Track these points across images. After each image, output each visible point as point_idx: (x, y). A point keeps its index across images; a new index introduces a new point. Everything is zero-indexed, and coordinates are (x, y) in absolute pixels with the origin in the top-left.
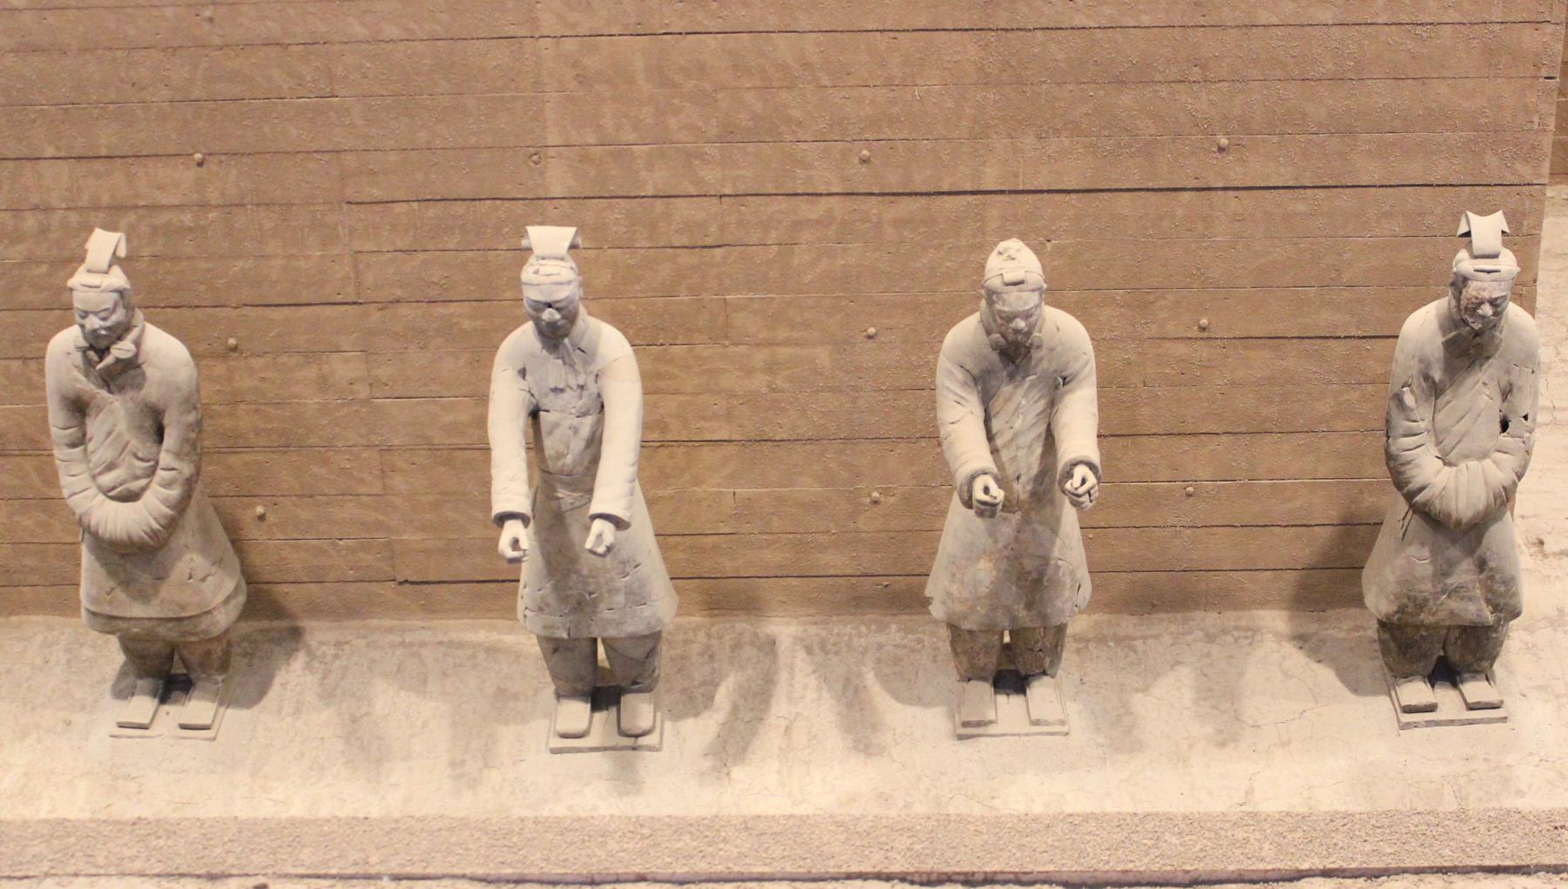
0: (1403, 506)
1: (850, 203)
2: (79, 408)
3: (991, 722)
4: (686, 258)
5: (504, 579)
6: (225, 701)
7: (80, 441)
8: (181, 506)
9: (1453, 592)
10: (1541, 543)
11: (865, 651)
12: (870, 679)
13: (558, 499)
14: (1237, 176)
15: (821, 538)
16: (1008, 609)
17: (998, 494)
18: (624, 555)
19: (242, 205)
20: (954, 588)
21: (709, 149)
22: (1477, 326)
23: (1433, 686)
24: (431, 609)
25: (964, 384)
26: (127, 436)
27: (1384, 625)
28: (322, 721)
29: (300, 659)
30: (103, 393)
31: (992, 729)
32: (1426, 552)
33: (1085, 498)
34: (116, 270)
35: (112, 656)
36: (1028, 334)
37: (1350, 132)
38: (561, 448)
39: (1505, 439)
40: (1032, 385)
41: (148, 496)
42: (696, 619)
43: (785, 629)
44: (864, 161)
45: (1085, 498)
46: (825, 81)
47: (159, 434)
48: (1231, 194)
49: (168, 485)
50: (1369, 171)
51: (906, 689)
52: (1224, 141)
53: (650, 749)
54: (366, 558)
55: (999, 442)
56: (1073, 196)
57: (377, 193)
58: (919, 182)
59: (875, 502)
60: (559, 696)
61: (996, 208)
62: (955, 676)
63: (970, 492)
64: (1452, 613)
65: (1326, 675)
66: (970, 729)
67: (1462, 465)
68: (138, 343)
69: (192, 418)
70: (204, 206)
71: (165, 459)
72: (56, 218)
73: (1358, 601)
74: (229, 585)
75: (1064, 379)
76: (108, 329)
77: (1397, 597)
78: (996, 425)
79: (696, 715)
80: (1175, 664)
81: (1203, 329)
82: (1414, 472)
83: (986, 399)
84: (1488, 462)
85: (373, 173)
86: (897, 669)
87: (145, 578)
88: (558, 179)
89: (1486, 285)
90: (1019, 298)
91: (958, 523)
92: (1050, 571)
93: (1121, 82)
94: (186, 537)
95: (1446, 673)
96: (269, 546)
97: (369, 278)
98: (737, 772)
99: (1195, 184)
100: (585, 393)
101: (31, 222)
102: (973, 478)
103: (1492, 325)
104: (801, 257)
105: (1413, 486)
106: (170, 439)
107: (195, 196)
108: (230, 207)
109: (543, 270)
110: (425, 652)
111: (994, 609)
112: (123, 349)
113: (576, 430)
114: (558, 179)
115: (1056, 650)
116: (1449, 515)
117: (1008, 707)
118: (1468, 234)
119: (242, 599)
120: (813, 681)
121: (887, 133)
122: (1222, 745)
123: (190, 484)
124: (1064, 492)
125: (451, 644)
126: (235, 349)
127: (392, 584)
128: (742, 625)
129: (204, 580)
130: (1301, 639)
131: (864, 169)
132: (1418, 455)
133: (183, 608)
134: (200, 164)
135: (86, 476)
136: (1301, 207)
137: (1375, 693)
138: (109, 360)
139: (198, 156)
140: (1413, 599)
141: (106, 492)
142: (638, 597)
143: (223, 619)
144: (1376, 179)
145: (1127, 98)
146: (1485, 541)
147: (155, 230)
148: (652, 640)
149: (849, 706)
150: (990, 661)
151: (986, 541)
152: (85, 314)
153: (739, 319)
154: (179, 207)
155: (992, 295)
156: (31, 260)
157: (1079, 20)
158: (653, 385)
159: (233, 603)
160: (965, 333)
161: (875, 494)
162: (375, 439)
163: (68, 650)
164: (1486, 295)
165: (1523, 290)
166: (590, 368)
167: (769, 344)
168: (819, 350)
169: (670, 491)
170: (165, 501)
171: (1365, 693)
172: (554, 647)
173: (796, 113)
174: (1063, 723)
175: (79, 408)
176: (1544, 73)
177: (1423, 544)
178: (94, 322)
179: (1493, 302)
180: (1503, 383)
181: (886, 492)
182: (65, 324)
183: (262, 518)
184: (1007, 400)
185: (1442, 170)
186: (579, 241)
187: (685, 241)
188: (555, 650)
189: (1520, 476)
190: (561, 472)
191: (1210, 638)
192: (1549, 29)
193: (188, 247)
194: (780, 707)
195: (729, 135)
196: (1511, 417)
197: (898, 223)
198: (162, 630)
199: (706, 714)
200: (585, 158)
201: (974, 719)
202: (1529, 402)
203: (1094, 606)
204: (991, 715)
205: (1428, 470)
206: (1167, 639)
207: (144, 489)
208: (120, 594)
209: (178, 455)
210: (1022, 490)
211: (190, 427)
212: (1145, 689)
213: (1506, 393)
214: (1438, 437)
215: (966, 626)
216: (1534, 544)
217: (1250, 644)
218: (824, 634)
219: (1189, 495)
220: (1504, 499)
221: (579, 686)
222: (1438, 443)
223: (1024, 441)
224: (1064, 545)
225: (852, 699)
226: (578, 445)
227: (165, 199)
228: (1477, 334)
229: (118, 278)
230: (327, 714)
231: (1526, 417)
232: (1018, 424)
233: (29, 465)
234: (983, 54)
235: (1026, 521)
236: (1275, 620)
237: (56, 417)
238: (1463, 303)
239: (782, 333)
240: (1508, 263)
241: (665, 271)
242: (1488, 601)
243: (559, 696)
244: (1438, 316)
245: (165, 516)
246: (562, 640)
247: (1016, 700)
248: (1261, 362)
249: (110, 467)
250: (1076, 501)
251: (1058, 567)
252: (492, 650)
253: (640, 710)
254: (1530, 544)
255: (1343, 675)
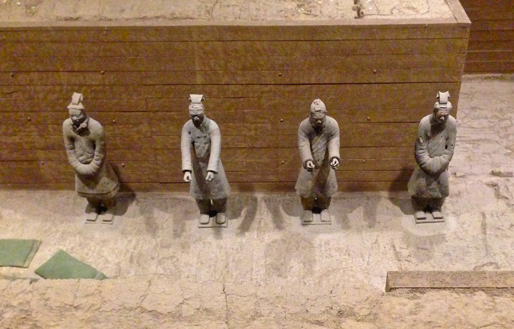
0: (419, 168)
1: (277, 87)
2: (72, 140)
3: (311, 221)
4: (232, 100)
5: (185, 186)
6: (115, 214)
7: (73, 148)
8: (101, 165)
9: (431, 190)
10: (455, 174)
11: (280, 201)
12: (281, 208)
13: (199, 165)
14: (379, 80)
15: (269, 173)
16: (316, 193)
17: (313, 166)
18: (217, 179)
19: (115, 85)
20: (302, 188)
21: (238, 72)
22: (440, 122)
23: (425, 212)
24: (169, 189)
25: (305, 137)
26: (86, 147)
27: (413, 197)
28: (140, 219)
29: (134, 203)
30: (79, 136)
31: (312, 223)
32: (424, 180)
33: (336, 167)
34: (80, 104)
35: (85, 202)
36: (322, 124)
37: (409, 68)
38: (200, 152)
39: (446, 151)
40: (323, 136)
41: (92, 163)
42: (237, 193)
43: (259, 196)
44: (280, 76)
45: (336, 167)
46: (270, 54)
47: (94, 147)
48: (376, 85)
49: (97, 160)
50: (414, 79)
51: (290, 213)
52: (375, 71)
53: (225, 227)
54: (152, 177)
55: (314, 151)
56: (335, 85)
57: (151, 83)
58: (295, 80)
59: (283, 163)
60: (201, 213)
61: (315, 88)
62: (302, 208)
63: (306, 165)
64: (431, 195)
65: (397, 209)
66: (306, 223)
67: (435, 158)
68: (87, 123)
69: (103, 143)
70: (105, 85)
71: (96, 153)
72: (65, 87)
73: (407, 190)
74: (115, 185)
75: (331, 135)
76: (79, 120)
77: (417, 190)
78: (313, 147)
79: (236, 218)
80: (359, 205)
81: (368, 120)
82: (422, 159)
83: (311, 141)
84: (441, 157)
85: (149, 77)
86: (288, 206)
87: (93, 184)
88: (199, 79)
89: (443, 111)
90: (319, 115)
91: (303, 173)
92: (327, 184)
93: (348, 55)
94: (103, 173)
95: (429, 209)
96: (126, 173)
97: (150, 105)
98: (247, 234)
99: (367, 82)
100: (206, 138)
101: (58, 88)
102: (307, 161)
103: (444, 122)
104: (263, 101)
105: (421, 163)
106: (97, 148)
107: (102, 82)
108: (111, 86)
109: (194, 107)
110: (167, 201)
111: (312, 193)
112: (83, 125)
113: (204, 148)
114: (199, 79)
115: (328, 204)
116: (431, 170)
117: (316, 216)
118: (439, 98)
119: (118, 188)
120: (266, 209)
121: (286, 68)
122: (370, 227)
123: (103, 160)
124: (330, 165)
125: (174, 199)
126: (115, 123)
127: (158, 183)
128: (249, 194)
129: (108, 184)
130: (392, 199)
131: (280, 78)
132: (423, 155)
133: (103, 191)
134: (103, 74)
135: (75, 157)
136: (395, 88)
137: (410, 214)
138: (80, 128)
139: (102, 72)
140: (421, 192)
141: (81, 162)
142: (221, 189)
143: (113, 194)
144: (415, 81)
145: (349, 59)
146: (440, 178)
147: (92, 91)
148: (224, 201)
149: (275, 216)
150: (311, 205)
151: (311, 176)
152: (72, 116)
153: (247, 116)
154: (99, 85)
155: (312, 114)
156: (58, 99)
157: (338, 38)
158: (224, 133)
159: (116, 189)
160: (305, 122)
161: (283, 161)
162: (153, 146)
163: (74, 199)
164: (443, 114)
165: (453, 112)
166: (207, 132)
167: (255, 123)
168: (268, 125)
169: (230, 160)
170: (97, 164)
171: (408, 214)
172: (200, 202)
173: (262, 63)
174: (330, 221)
175: (72, 140)
176: (462, 52)
177: (424, 178)
178: (75, 118)
179: (445, 116)
180: (447, 137)
181: (285, 161)
182: (67, 117)
183: (124, 166)
184: (317, 140)
185: (434, 78)
186: (204, 98)
187: (233, 96)
188: (200, 202)
189: (450, 160)
190: (200, 158)
191: (368, 198)
192: (464, 40)
193: (100, 96)
194: (257, 217)
195: (244, 68)
196: (448, 145)
197: (289, 92)
198: (98, 197)
199: (239, 218)
200: (206, 74)
201: (307, 220)
202: (453, 141)
203: (338, 191)
204: (311, 219)
205: (426, 159)
206: (357, 199)
207: (91, 161)
208: (86, 188)
209: (100, 153)
210: (319, 163)
211: (102, 145)
212: (351, 212)
213: (447, 139)
214: (429, 150)
215: (305, 197)
216: (453, 174)
217: (379, 200)
218: (269, 196)
219: (364, 162)
220: (445, 167)
221: (206, 211)
222: (428, 152)
223: (320, 151)
224: (330, 177)
225: (276, 214)
226: (204, 151)
227: (93, 83)
228: (440, 124)
229: (81, 106)
230: (142, 217)
231: (452, 145)
232: (319, 146)
233: (61, 152)
234: (311, 47)
235: (321, 171)
236: (385, 194)
237: (67, 143)
238: (437, 116)
239: (259, 120)
240: (449, 105)
241: (228, 104)
242: (440, 192)
243: (201, 213)
244: (430, 118)
245: (97, 168)
246: (201, 200)
247: (318, 215)
248: (383, 129)
249: (81, 155)
250: (333, 167)
251: (329, 183)
252: (184, 200)
253: (222, 217)
254: (452, 174)
255: (403, 209)
